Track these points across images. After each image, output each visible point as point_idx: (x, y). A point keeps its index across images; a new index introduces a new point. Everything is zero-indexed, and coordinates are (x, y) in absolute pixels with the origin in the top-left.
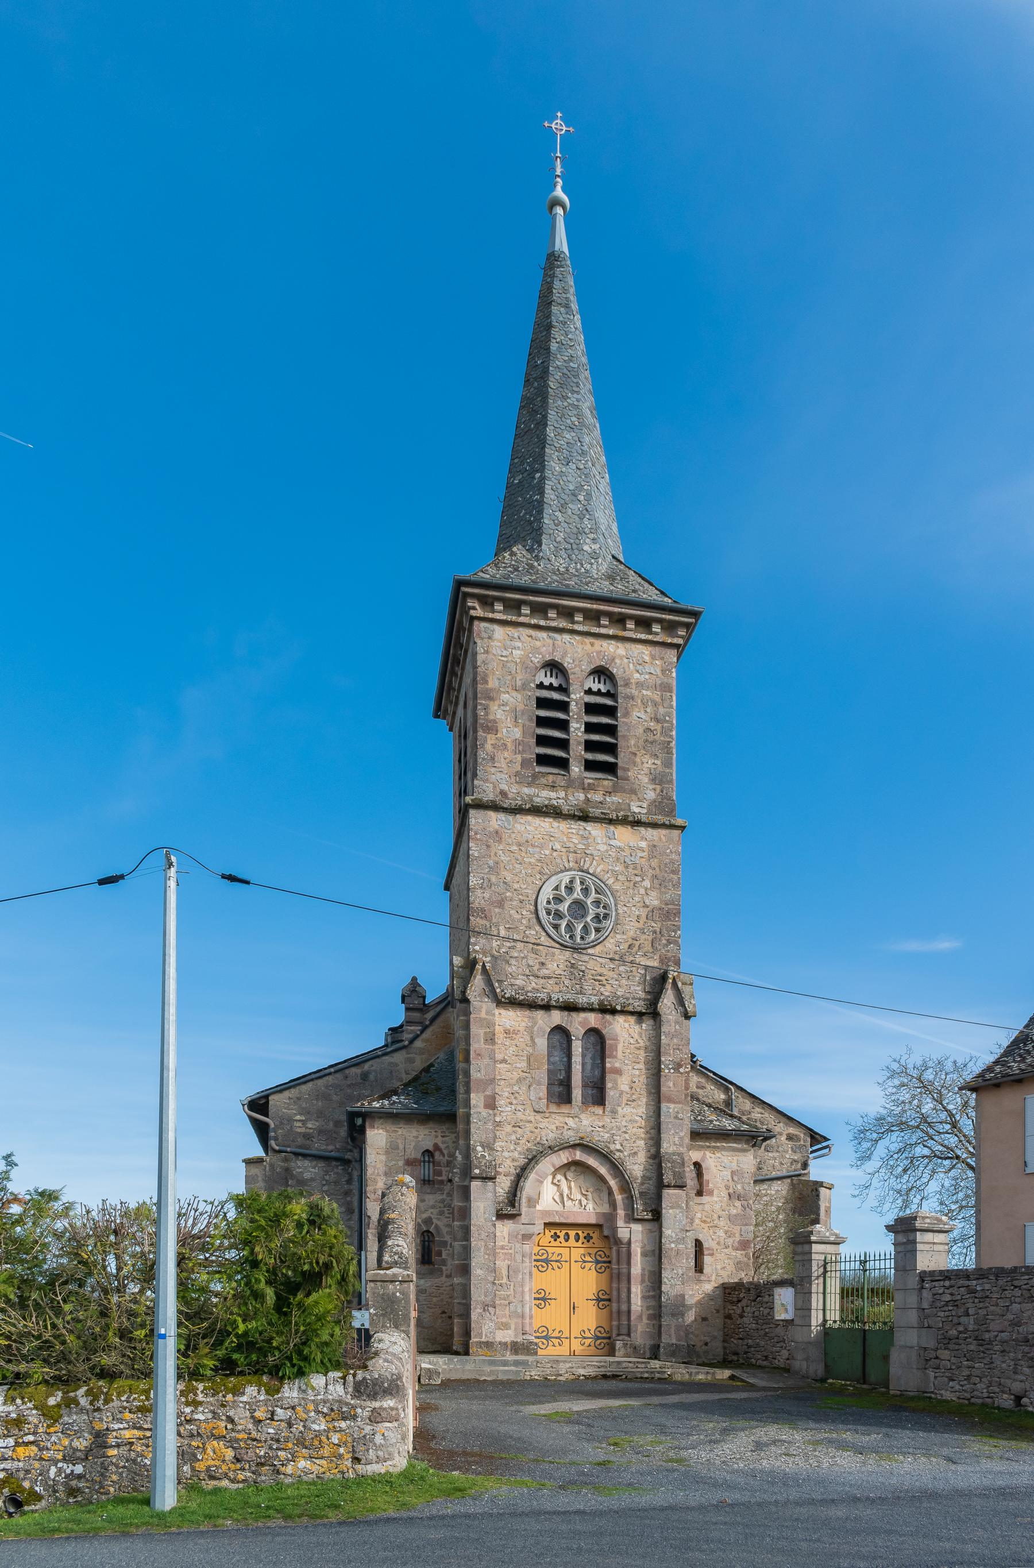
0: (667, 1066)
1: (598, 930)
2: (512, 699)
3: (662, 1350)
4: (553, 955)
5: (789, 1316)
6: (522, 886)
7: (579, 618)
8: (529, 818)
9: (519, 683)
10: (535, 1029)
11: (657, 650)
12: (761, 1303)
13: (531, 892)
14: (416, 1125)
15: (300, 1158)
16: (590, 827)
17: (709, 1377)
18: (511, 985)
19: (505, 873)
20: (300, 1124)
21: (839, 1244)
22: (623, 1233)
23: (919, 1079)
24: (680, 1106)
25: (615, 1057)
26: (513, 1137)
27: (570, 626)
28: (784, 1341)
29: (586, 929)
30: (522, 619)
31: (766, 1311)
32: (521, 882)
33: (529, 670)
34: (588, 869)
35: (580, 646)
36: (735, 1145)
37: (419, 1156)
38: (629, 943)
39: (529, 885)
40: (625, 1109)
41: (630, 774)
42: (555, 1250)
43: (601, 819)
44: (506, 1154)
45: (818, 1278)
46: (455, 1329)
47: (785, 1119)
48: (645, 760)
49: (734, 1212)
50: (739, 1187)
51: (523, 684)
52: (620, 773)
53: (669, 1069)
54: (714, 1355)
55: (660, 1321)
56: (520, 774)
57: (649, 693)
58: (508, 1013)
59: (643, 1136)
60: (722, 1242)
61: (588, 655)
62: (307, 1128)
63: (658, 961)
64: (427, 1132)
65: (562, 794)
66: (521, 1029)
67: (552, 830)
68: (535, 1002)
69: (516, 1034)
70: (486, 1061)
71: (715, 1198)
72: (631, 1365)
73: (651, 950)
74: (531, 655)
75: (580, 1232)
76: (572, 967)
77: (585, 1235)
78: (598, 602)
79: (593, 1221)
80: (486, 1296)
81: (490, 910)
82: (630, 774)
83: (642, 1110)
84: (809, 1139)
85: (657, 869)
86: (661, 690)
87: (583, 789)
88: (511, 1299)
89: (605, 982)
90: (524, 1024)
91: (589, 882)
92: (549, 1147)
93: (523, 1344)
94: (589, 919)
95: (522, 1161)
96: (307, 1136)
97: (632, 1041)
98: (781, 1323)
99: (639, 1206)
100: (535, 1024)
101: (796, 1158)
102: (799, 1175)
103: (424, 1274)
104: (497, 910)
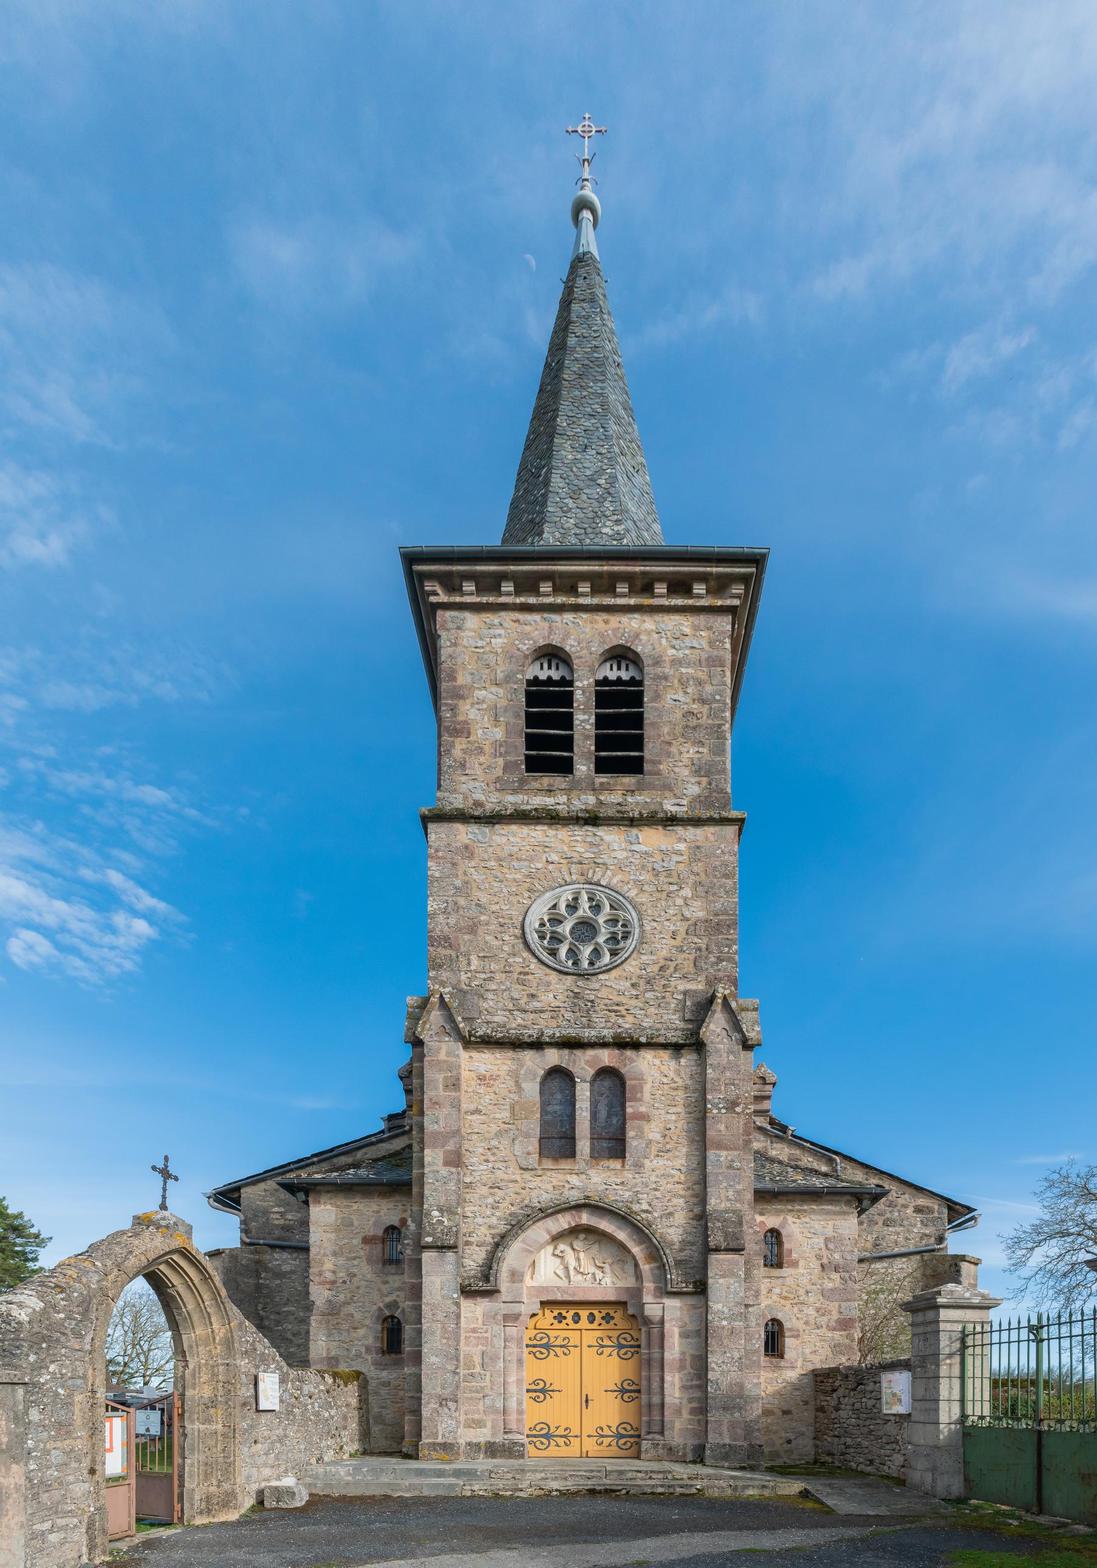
0: (715, 1105)
1: (614, 953)
2: (491, 696)
3: (708, 1452)
4: (549, 984)
5: (900, 1409)
6: (503, 907)
7: (584, 588)
8: (514, 828)
9: (500, 676)
10: (522, 1072)
11: (702, 619)
12: (864, 1392)
13: (517, 913)
14: (376, 1199)
15: (277, 1250)
17: (767, 1493)
18: (487, 1023)
20: (278, 1216)
21: (988, 1308)
22: (652, 1309)
23: (1085, 1187)
24: (736, 1153)
25: (641, 1100)
26: (490, 1200)
27: (572, 600)
28: (897, 1442)
29: (597, 953)
30: (503, 600)
31: (871, 1403)
32: (502, 902)
33: (514, 660)
34: (599, 880)
35: (589, 626)
36: (830, 1207)
37: (380, 1233)
38: (660, 965)
39: (513, 905)
40: (655, 1162)
41: (661, 767)
42: (557, 1335)
43: (617, 819)
44: (479, 1220)
45: (950, 1355)
46: (406, 1428)
47: (910, 1190)
48: (684, 750)
49: (830, 1285)
50: (837, 1256)
51: (506, 677)
52: (647, 767)
53: (720, 1109)
54: (801, 1455)
55: (707, 1416)
56: (503, 780)
57: (690, 671)
58: (483, 1055)
59: (682, 1193)
60: (812, 1321)
61: (601, 635)
62: (286, 1219)
63: (703, 983)
64: (391, 1206)
67: (547, 839)
68: (519, 1039)
69: (495, 1080)
70: (446, 1110)
71: (801, 1270)
72: (639, 1475)
73: (692, 970)
74: (517, 642)
75: (596, 1312)
76: (575, 998)
77: (603, 1314)
78: (611, 563)
79: (611, 1297)
80: (443, 1388)
82: (661, 767)
83: (680, 1162)
84: (946, 1211)
85: (703, 875)
86: (708, 666)
87: (594, 790)
88: (488, 1391)
89: (624, 1013)
90: (505, 1068)
91: (601, 896)
92: (540, 1209)
93: (504, 1445)
94: (601, 939)
95: (502, 1228)
96: (286, 1228)
97: (665, 1080)
98: (892, 1418)
99: (674, 1276)
101: (927, 1232)
102: (933, 1250)
103: (386, 1365)
104: (467, 937)
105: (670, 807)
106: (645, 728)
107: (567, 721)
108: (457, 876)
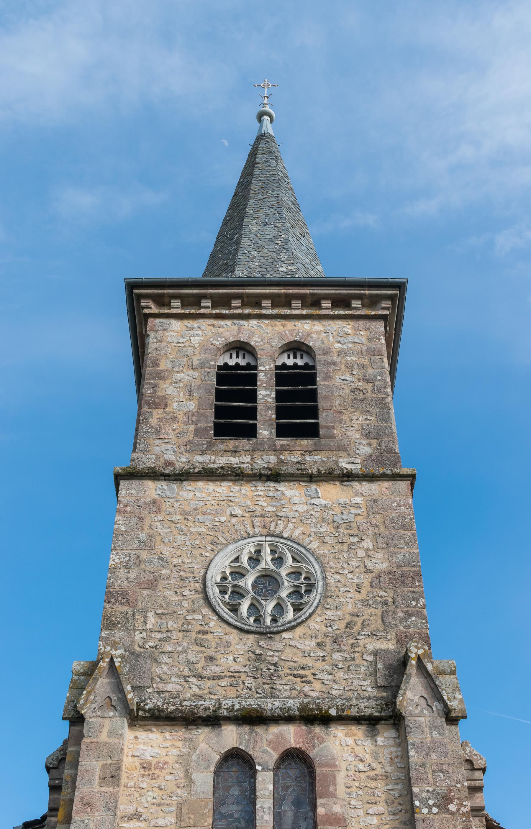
0: (425, 802)
1: (297, 608)
2: (187, 377)
8: (201, 484)
9: (196, 362)
10: (194, 757)
11: (360, 324)
16: (283, 487)
18: (159, 692)
19: (162, 547)
25: (333, 795)
27: (257, 311)
29: (279, 608)
30: (202, 311)
32: (184, 555)
38: (346, 621)
39: (196, 558)
41: (335, 431)
43: (297, 476)
51: (201, 364)
52: (322, 431)
53: (430, 807)
57: (354, 358)
58: (151, 735)
61: (280, 334)
63: (394, 641)
65: (248, 458)
66: (170, 760)
68: (193, 713)
70: (99, 814)
73: (381, 627)
74: (211, 339)
76: (257, 660)
78: (287, 288)
81: (135, 593)
82: (335, 431)
85: (381, 527)
87: (275, 451)
89: (310, 678)
90: (175, 751)
94: (284, 593)
100: (194, 749)
104: (146, 592)
105: (345, 464)
106: (320, 400)
107: (252, 396)
108: (143, 529)
